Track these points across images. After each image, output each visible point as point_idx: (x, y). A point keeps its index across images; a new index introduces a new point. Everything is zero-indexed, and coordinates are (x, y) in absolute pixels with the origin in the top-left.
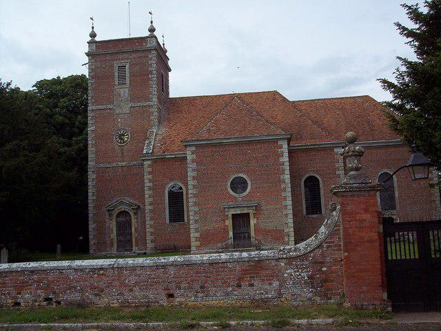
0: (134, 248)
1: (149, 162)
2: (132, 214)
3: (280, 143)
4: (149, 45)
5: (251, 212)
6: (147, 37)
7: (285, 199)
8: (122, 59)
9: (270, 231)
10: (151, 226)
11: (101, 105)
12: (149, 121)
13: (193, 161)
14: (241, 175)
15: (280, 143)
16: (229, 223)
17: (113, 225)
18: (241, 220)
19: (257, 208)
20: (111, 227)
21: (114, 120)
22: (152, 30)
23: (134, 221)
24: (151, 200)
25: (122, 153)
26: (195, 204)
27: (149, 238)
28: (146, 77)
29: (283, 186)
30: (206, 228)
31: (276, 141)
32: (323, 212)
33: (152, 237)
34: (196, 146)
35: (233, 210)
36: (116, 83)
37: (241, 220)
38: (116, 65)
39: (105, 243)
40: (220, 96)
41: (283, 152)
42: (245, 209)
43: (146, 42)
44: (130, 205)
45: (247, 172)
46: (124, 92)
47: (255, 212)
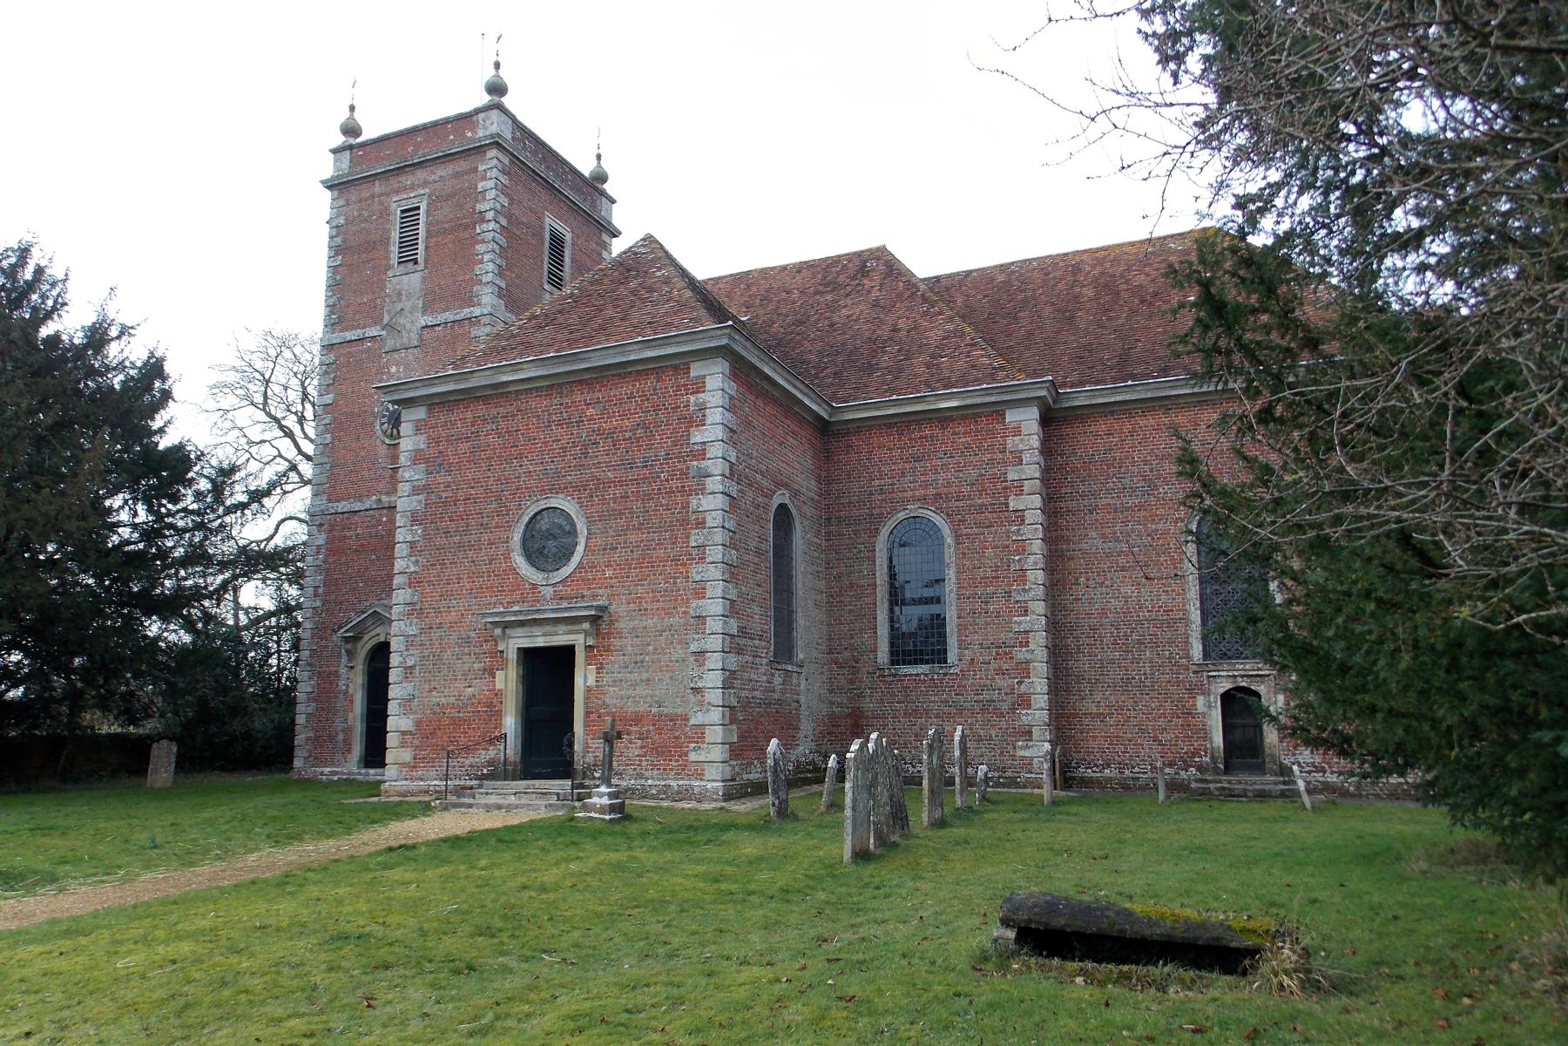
3: (696, 370)
4: (481, 133)
6: (477, 111)
7: (700, 593)
8: (413, 187)
15: (696, 370)
16: (508, 681)
18: (548, 673)
22: (497, 89)
30: (436, 698)
31: (679, 364)
32: (952, 656)
35: (519, 632)
36: (394, 260)
37: (548, 673)
39: (332, 738)
41: (702, 408)
42: (562, 628)
46: (411, 281)
47: (590, 642)
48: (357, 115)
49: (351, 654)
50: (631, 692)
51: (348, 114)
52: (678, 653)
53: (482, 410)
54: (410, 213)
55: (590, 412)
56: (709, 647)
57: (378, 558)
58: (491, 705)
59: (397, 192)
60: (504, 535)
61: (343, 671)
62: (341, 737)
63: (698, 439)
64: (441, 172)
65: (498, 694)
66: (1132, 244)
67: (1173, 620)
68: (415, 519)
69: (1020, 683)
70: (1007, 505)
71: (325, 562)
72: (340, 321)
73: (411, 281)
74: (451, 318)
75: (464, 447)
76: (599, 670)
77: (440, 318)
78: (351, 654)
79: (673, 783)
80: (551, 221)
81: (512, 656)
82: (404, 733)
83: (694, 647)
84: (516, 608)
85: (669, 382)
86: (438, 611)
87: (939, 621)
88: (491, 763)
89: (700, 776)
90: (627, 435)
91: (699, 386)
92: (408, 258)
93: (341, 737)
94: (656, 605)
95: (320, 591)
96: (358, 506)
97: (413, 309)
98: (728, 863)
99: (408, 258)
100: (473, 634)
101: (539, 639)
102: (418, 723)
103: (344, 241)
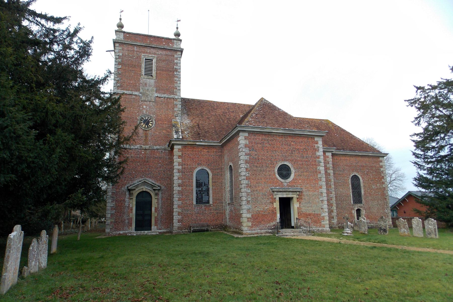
0: (153, 227)
1: (180, 147)
2: (153, 194)
3: (316, 139)
4: (175, 46)
5: (295, 196)
7: (321, 187)
8: (150, 53)
9: (310, 215)
10: (179, 206)
11: (127, 90)
12: (174, 112)
13: (246, 146)
14: (286, 163)
16: (277, 205)
17: (133, 204)
18: (285, 204)
19: (300, 194)
20: (131, 206)
21: (139, 106)
23: (154, 201)
24: (180, 181)
25: (146, 137)
26: (248, 186)
27: (176, 217)
28: (171, 73)
29: (319, 176)
30: (257, 209)
31: (313, 137)
33: (180, 217)
34: (249, 132)
35: (279, 193)
37: (285, 204)
38: (143, 57)
39: (123, 222)
40: (225, 103)
41: (318, 147)
42: (291, 193)
43: (173, 43)
44: (152, 186)
45: (291, 161)
48: (122, 21)
49: (131, 194)
51: (119, 21)
52: (317, 200)
53: (264, 137)
54: (149, 61)
57: (141, 165)
58: (273, 211)
59: (144, 53)
60: (273, 169)
61: (127, 200)
62: (127, 221)
63: (318, 154)
64: (164, 52)
65: (275, 208)
66: (307, 119)
67: (348, 196)
68: (246, 162)
72: (121, 86)
73: (151, 82)
74: (167, 96)
76: (300, 203)
77: (163, 96)
78: (131, 194)
79: (320, 229)
81: (278, 199)
82: (248, 218)
83: (321, 199)
84: (277, 188)
85: (310, 140)
86: (256, 187)
88: (274, 225)
89: (324, 227)
91: (317, 143)
93: (127, 221)
97: (152, 90)
99: (149, 72)
100: (266, 193)
101: (285, 195)
102: (252, 216)
103: (122, 61)
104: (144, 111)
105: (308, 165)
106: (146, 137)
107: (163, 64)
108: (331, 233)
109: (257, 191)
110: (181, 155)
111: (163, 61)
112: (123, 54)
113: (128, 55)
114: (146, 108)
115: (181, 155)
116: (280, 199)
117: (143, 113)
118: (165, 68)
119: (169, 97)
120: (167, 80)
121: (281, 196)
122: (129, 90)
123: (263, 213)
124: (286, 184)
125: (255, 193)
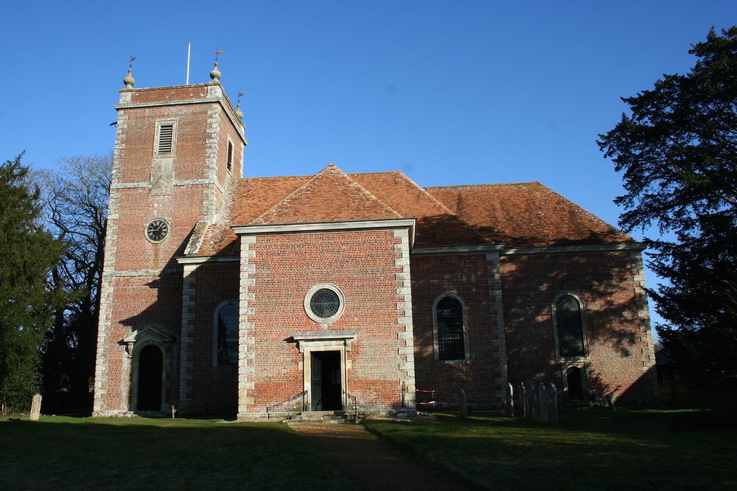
3: (397, 233)
8: (168, 116)
9: (374, 383)
24: (191, 328)
25: (156, 255)
28: (200, 143)
30: (265, 374)
50: (370, 372)
54: (167, 128)
55: (344, 247)
56: (407, 352)
69: (496, 367)
70: (488, 294)
71: (113, 302)
73: (167, 162)
74: (191, 183)
75: (276, 258)
76: (354, 361)
80: (229, 139)
81: (307, 356)
86: (265, 333)
87: (462, 340)
90: (363, 259)
92: (165, 149)
94: (380, 334)
95: (110, 317)
96: (134, 273)
98: (511, 439)
99: (165, 149)
101: (321, 347)
104: (155, 212)
105: (374, 287)
106: (156, 255)
107: (189, 129)
108: (438, 422)
109: (266, 340)
110: (194, 282)
111: (189, 124)
112: (128, 126)
113: (136, 125)
114: (158, 206)
115: (194, 282)
116: (313, 354)
117: (153, 216)
118: (191, 135)
119: (195, 183)
120: (193, 155)
121: (341, 351)
122: (134, 181)
123: (276, 381)
124: (325, 326)
125: (264, 344)
